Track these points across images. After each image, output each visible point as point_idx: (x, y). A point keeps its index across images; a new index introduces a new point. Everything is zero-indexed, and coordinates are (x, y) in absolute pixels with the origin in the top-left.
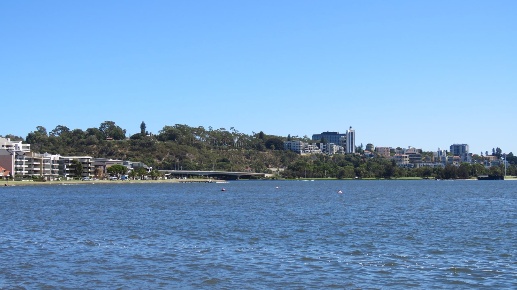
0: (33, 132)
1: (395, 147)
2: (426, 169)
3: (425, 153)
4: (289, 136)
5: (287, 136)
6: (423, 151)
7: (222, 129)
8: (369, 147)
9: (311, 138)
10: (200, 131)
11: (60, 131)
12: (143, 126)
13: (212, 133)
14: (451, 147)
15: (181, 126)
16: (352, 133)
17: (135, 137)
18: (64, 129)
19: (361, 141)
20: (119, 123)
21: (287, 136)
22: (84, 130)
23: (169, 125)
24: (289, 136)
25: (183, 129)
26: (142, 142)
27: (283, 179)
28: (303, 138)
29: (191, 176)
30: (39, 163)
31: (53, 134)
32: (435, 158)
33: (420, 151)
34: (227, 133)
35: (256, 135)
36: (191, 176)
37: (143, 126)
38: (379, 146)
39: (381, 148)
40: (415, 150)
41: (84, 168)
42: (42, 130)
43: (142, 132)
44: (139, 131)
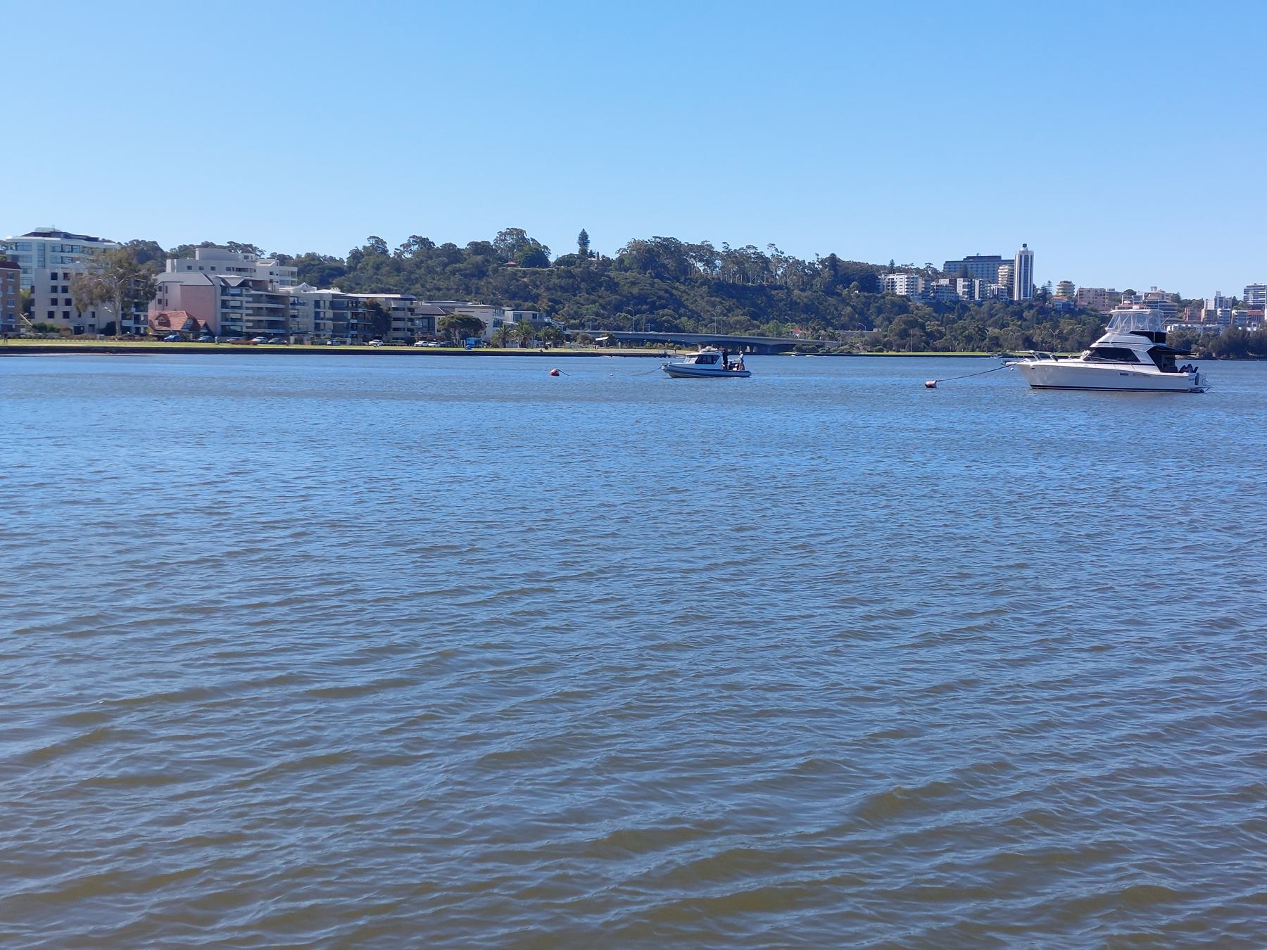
0: (360, 248)
1: (1120, 289)
2: (1181, 336)
3: (1188, 303)
4: (892, 263)
5: (887, 264)
6: (1183, 297)
7: (749, 247)
8: (1067, 287)
9: (941, 269)
10: (704, 252)
11: (415, 248)
12: (584, 239)
13: (730, 256)
14: (1246, 291)
15: (665, 239)
16: (1027, 257)
17: (567, 261)
18: (424, 242)
19: (1046, 276)
20: (536, 233)
21: (887, 264)
22: (462, 245)
23: (639, 238)
24: (892, 263)
25: (669, 248)
26: (585, 273)
27: (613, 351)
28: (922, 267)
29: (245, 318)
30: (281, 306)
31: (402, 253)
32: (1209, 312)
33: (1176, 298)
34: (760, 257)
35: (822, 262)
36: (245, 318)
37: (584, 239)
38: (1086, 286)
39: (1089, 291)
40: (1163, 295)
41: (396, 319)
42: (378, 246)
43: (583, 251)
44: (575, 250)
